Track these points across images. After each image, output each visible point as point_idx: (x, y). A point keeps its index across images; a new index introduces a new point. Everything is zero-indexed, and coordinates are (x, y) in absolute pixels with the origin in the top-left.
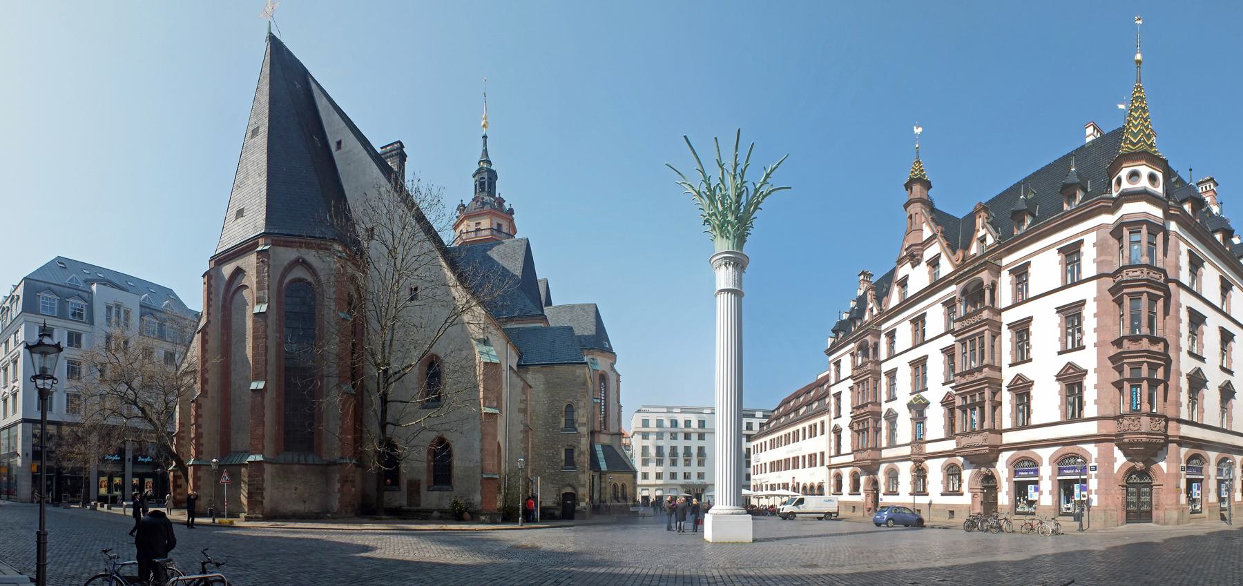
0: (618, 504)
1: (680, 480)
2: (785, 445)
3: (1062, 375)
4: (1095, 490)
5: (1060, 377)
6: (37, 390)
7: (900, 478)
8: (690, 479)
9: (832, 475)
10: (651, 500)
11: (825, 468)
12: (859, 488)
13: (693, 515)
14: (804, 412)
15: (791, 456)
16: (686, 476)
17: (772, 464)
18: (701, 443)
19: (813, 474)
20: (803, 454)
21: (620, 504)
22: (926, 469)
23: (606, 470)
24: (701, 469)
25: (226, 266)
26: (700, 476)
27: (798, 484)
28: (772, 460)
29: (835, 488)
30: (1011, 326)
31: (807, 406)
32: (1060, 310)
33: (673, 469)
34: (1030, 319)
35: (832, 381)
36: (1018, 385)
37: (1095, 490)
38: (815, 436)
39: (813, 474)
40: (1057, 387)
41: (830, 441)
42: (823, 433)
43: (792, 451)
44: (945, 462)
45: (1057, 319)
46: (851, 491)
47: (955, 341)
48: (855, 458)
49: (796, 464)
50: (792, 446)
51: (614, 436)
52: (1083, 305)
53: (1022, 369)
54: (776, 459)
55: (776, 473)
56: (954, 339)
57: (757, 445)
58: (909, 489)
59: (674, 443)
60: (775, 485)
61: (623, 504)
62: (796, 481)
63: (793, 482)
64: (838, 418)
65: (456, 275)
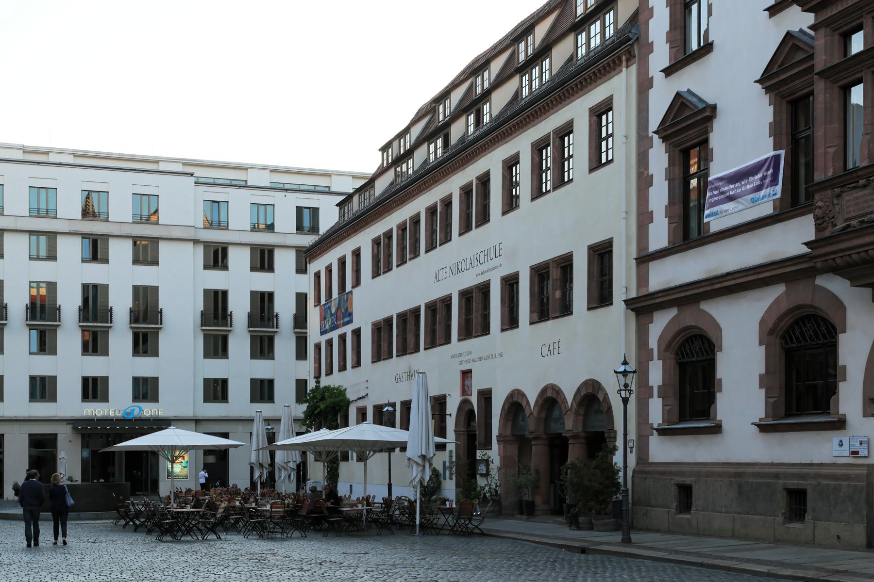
3: (777, 74)
6: (621, 398)
9: (653, 343)
12: (833, 390)
15: (453, 287)
18: (145, 276)
19: (554, 349)
23: (816, 283)
24: (145, 367)
27: (486, 396)
28: (381, 315)
29: (674, 402)
33: (95, 366)
39: (554, 349)
41: (644, 181)
42: (596, 163)
43: (457, 269)
49: (476, 316)
54: (393, 309)
55: (397, 364)
57: (329, 270)
62: (477, 384)
63: (465, 390)
65: (224, 514)
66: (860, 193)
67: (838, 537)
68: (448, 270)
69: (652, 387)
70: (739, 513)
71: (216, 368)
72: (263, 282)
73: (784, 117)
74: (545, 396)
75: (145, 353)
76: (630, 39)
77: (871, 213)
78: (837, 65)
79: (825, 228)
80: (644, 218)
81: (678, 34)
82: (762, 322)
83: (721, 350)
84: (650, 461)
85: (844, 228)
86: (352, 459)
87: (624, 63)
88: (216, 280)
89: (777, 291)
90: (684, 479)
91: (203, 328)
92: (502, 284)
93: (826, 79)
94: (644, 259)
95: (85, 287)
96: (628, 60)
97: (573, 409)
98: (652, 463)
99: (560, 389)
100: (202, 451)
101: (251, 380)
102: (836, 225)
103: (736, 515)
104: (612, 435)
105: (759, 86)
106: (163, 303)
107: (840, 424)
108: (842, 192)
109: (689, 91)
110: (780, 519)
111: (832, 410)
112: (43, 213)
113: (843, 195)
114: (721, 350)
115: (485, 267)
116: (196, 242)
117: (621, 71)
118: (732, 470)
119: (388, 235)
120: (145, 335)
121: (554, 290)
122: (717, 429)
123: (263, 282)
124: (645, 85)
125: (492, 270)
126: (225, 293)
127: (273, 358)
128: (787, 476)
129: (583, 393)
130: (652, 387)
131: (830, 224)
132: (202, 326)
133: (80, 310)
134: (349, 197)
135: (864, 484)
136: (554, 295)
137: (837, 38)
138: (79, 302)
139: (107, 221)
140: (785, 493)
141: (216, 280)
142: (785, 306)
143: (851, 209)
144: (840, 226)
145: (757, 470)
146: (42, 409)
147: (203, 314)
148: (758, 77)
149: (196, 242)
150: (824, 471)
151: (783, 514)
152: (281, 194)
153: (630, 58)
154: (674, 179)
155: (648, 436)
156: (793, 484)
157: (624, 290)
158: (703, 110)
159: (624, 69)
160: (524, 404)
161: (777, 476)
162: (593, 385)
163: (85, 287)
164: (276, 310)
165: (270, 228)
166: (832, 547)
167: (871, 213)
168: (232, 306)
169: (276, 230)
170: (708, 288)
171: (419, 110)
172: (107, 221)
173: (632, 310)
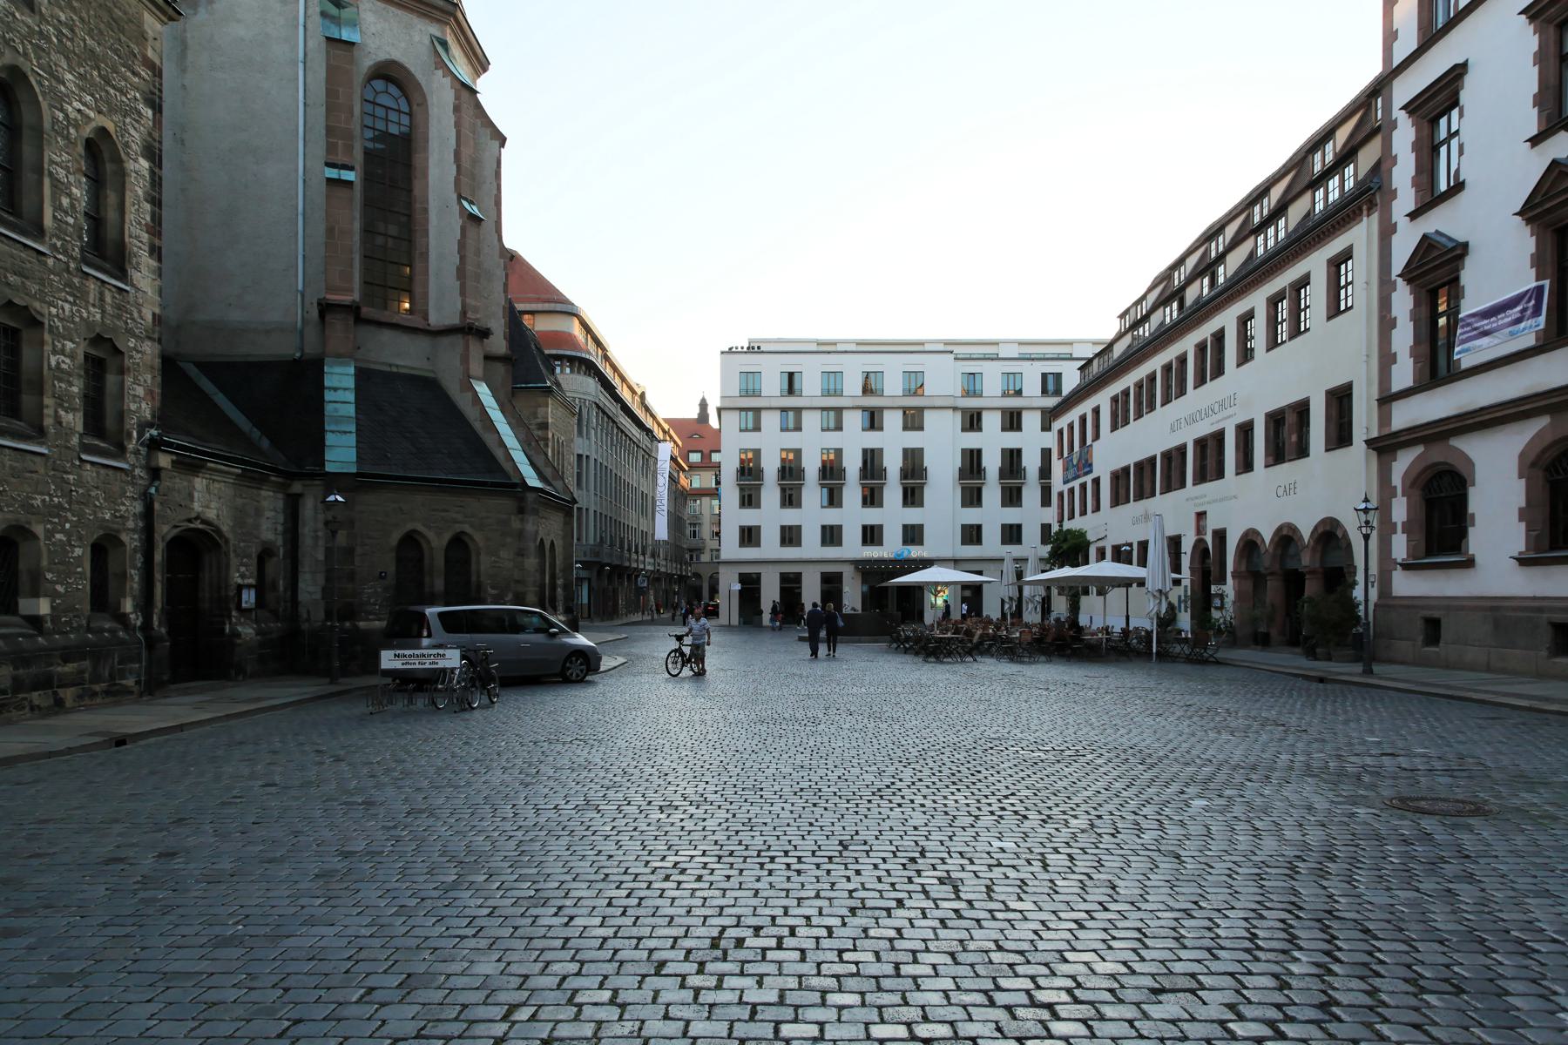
1: (852, 547)
4: (1395, 533)
7: (1478, 501)
9: (1397, 480)
10: (808, 608)
11: (1357, 453)
13: (1461, 180)
15: (1188, 437)
17: (1120, 477)
18: (913, 440)
19: (1290, 489)
20: (1242, 418)
22: (1465, 473)
24: (913, 516)
27: (1220, 536)
30: (1411, 108)
37: (1395, 533)
39: (1290, 489)
41: (1387, 324)
46: (1533, 541)
50: (1195, 398)
51: (446, 341)
54: (1130, 459)
55: (1134, 508)
58: (1516, 538)
59: (873, 440)
60: (1131, 545)
62: (1212, 524)
63: (1200, 530)
64: (1272, 348)
68: (1183, 420)
71: (972, 516)
72: (1012, 440)
80: (1387, 359)
81: (1425, 178)
82: (1522, 456)
84: (1394, 594)
88: (972, 440)
90: (1430, 612)
94: (1387, 400)
96: (1369, 209)
97: (1310, 547)
98: (1396, 597)
109: (1437, 232)
110: (1544, 653)
116: (955, 409)
117: (1362, 220)
120: (913, 490)
122: (1470, 563)
123: (1012, 440)
124: (1387, 231)
125: (1225, 418)
127: (1021, 506)
129: (1320, 530)
134: (1090, 361)
138: (860, 464)
149: (955, 409)
151: (1548, 648)
153: (1372, 206)
156: (1428, 613)
158: (1453, 249)
159: (1365, 219)
161: (1540, 610)
163: (865, 451)
164: (1024, 464)
165: (1019, 393)
173: (1374, 449)
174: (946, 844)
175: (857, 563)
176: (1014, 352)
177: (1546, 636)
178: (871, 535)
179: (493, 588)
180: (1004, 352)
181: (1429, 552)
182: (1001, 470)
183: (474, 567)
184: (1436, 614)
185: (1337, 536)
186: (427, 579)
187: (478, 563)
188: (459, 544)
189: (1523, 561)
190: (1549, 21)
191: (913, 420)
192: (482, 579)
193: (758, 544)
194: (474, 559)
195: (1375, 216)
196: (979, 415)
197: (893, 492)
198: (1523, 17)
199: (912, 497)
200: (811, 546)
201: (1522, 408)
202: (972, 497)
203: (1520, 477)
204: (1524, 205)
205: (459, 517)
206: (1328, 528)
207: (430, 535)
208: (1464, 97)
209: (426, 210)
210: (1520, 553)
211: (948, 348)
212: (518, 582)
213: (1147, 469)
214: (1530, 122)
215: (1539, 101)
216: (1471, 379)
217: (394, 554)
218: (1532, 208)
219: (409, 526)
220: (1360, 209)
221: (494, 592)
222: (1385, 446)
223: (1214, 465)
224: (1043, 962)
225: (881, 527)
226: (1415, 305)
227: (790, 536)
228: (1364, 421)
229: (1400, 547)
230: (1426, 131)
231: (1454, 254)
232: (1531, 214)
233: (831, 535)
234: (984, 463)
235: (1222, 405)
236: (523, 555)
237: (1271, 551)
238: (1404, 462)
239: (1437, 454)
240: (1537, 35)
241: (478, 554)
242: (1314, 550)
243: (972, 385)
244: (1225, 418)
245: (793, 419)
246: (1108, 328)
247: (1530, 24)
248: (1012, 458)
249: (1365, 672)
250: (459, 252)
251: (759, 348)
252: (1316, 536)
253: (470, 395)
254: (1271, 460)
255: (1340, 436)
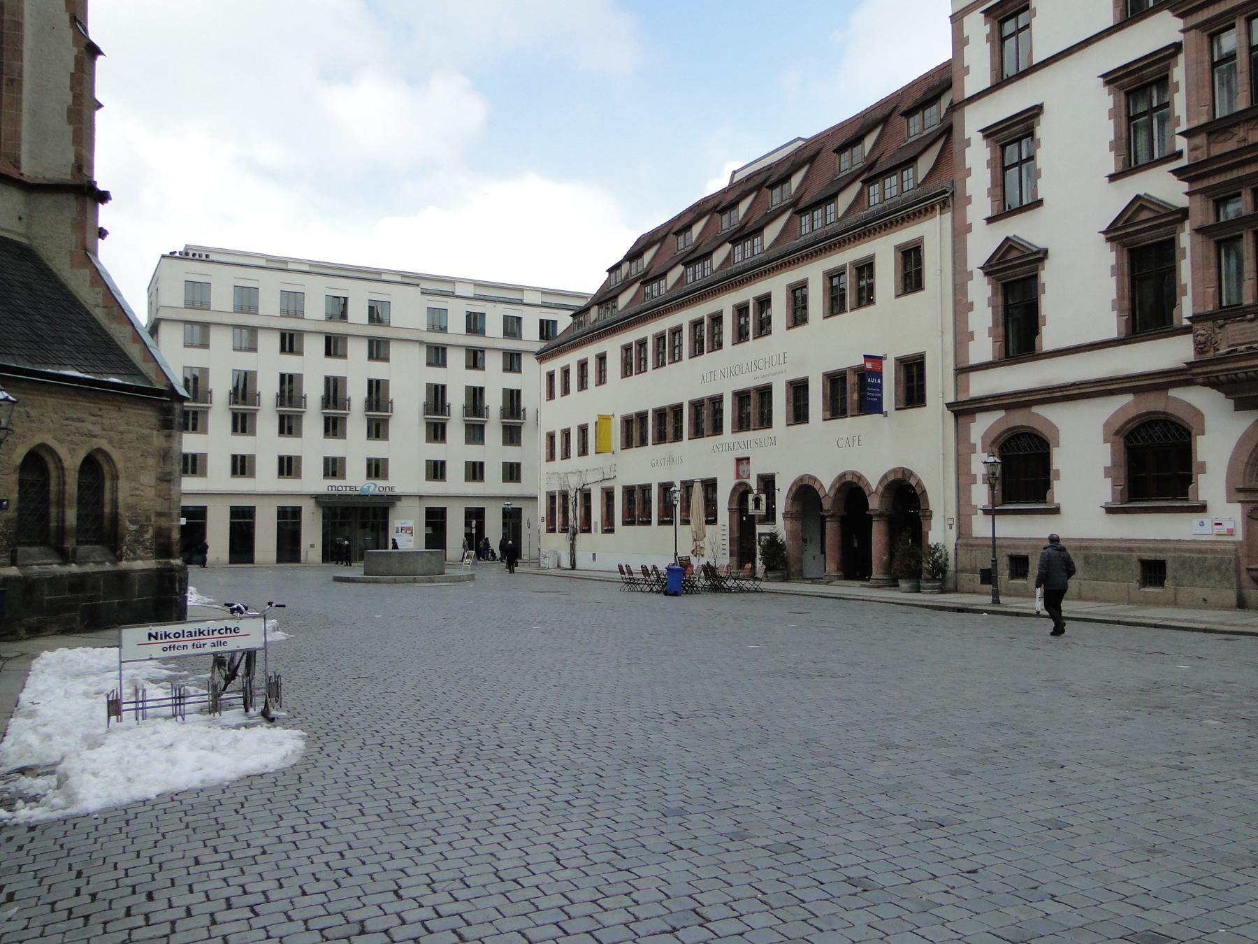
0: (57, 569)
1: (312, 481)
2: (659, 364)
5: (1117, 233)
8: (343, 476)
13: (1039, 198)
14: (777, 241)
15: (727, 389)
16: (333, 468)
18: (378, 370)
21: (74, 568)
24: (377, 449)
25: (62, 652)
26: (376, 468)
27: (768, 483)
28: (633, 409)
30: (989, 133)
31: (687, 265)
32: (1111, 79)
33: (243, 445)
34: (1037, 111)
35: (977, 77)
36: (1010, 260)
38: (680, 359)
40: (1106, 257)
41: (961, 307)
44: (1123, 409)
45: (1104, 100)
47: (1184, 31)
48: (1200, 348)
50: (731, 353)
51: (48, 201)
52: (1037, 115)
53: (1019, 228)
56: (1180, 24)
58: (1105, 491)
61: (90, 568)
66: (1246, 325)
67: (1204, 600)
68: (718, 373)
69: (975, 475)
70: (1085, 579)
71: (436, 451)
72: (475, 378)
73: (1126, 261)
74: (843, 480)
75: (335, 435)
76: (947, 192)
77: (1255, 342)
78: (1211, 226)
79: (1206, 352)
80: (962, 337)
81: (999, 190)
82: (1107, 425)
83: (1058, 446)
84: (974, 536)
85: (1229, 353)
86: (596, 531)
87: (938, 211)
88: (437, 376)
89: (1128, 399)
90: (1018, 551)
91: (466, 418)
92: (786, 386)
93: (1203, 234)
94: (963, 370)
95: (327, 379)
96: (941, 209)
97: (879, 493)
98: (976, 538)
99: (861, 475)
100: (707, 526)
101: (503, 463)
102: (1218, 350)
103: (1082, 582)
104: (928, 514)
105: (1102, 236)
106: (393, 394)
107: (1202, 508)
108: (1226, 323)
109: (1015, 236)
110: (1135, 585)
111: (1191, 496)
112: (291, 313)
113: (1227, 326)
114: (1058, 446)
115: (773, 370)
116: (421, 342)
117: (935, 216)
118: (1077, 544)
119: (642, 344)
120: (244, 416)
121: (852, 393)
122: (1056, 511)
123: (475, 378)
124: (960, 231)
125: (773, 375)
126: (519, 392)
128: (1140, 549)
129: (891, 478)
130: (975, 475)
131: (1212, 349)
132: (323, 409)
133: (277, 396)
134: (586, 310)
135: (1233, 557)
136: (852, 397)
137: (1211, 203)
138: (322, 392)
139: (389, 326)
140: (1139, 564)
141: (437, 376)
142: (1133, 413)
143: (1237, 337)
144: (1222, 351)
145: (1105, 544)
146: (474, 488)
147: (426, 405)
148: (1104, 228)
149: (421, 342)
150: (1184, 546)
151: (1138, 581)
152: (491, 305)
153: (944, 205)
154: (997, 306)
155: (970, 516)
156: (1147, 556)
157: (941, 395)
158: (1038, 252)
159: (938, 216)
160: (817, 487)
161: (1130, 550)
162: (903, 472)
163: (327, 379)
164: (448, 401)
165: (443, 330)
166: (1200, 608)
167: (1255, 342)
168: (449, 399)
169: (449, 331)
170: (1048, 396)
171: (638, 240)
172: (389, 326)
173: (952, 411)
174: (320, 800)
175: (318, 498)
176: (470, 291)
177: (1137, 571)
178: (333, 468)
179: (133, 522)
180: (460, 290)
181: (1005, 500)
182: (503, 409)
183: (107, 495)
184: (1023, 553)
185: (911, 485)
186: (53, 511)
187: (115, 490)
188: (93, 467)
189: (1110, 510)
190: (1121, 88)
191: (378, 350)
192: (119, 511)
193: (299, 476)
194: (108, 484)
195: (948, 216)
196: (444, 350)
197: (356, 422)
198: (1101, 80)
199: (377, 429)
200: (266, 478)
201: (1109, 387)
202: (437, 432)
203: (1105, 441)
204: (1109, 227)
205: (96, 429)
206: (900, 476)
207: (62, 451)
208: (1040, 132)
209: (19, 26)
210: (1106, 503)
211: (410, 280)
212: (160, 514)
213: (670, 419)
214: (1110, 164)
215: (1114, 146)
216: (1053, 359)
217: (15, 477)
218: (1114, 230)
219: (37, 440)
220: (933, 208)
221: (133, 527)
222: (963, 410)
223: (757, 416)
224: (523, 913)
225: (343, 459)
226: (993, 295)
227: (475, 471)
228: (938, 385)
229: (981, 495)
230: (999, 154)
231: (1038, 256)
232: (1113, 234)
233: (475, 471)
234: (449, 400)
235: (769, 362)
236: (169, 481)
237: (832, 495)
238: (982, 426)
239: (1019, 419)
240: (1112, 96)
241: (115, 477)
242: (883, 496)
243: (438, 321)
244: (773, 375)
245: (248, 338)
246: (591, 282)
247: (1104, 86)
248: (476, 396)
249: (994, 602)
250: (72, 89)
251: (207, 256)
252: (885, 483)
253: (86, 273)
254: (828, 415)
255: (913, 394)
